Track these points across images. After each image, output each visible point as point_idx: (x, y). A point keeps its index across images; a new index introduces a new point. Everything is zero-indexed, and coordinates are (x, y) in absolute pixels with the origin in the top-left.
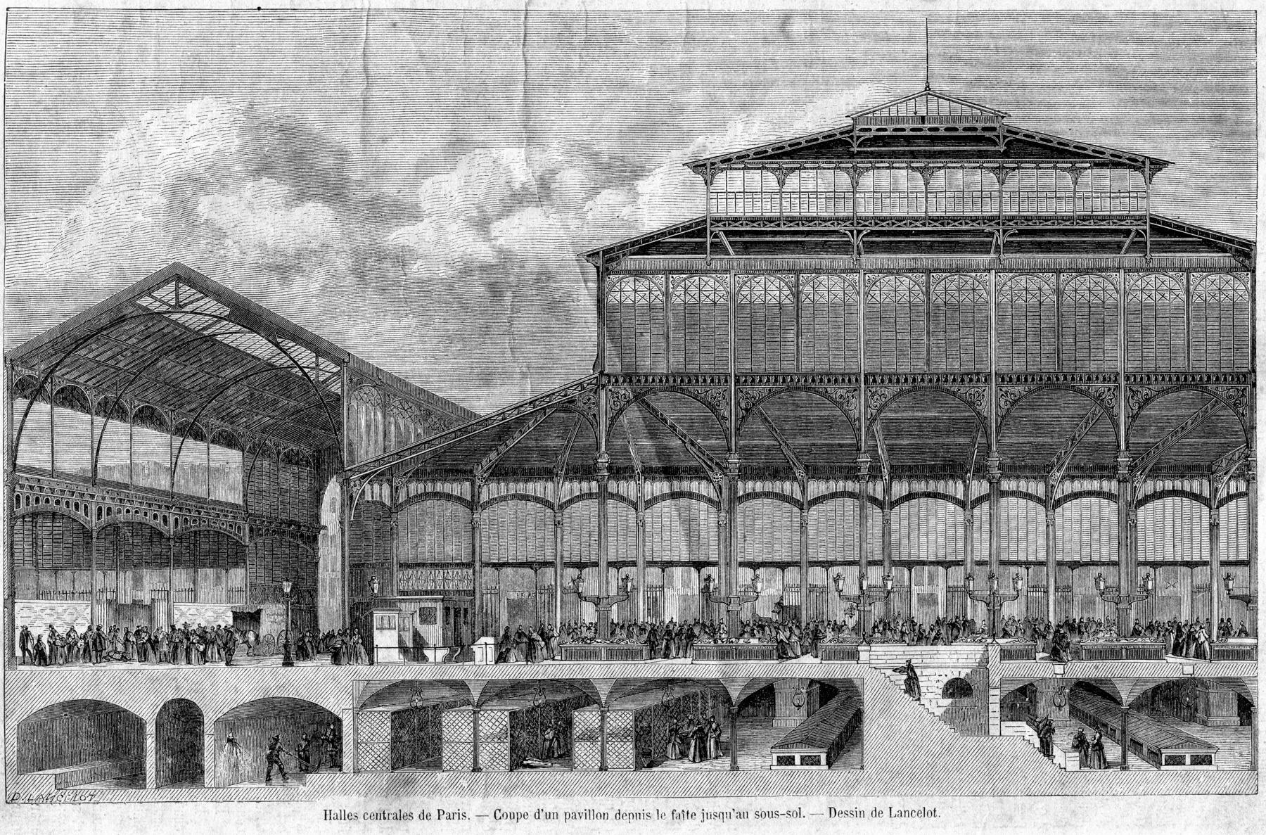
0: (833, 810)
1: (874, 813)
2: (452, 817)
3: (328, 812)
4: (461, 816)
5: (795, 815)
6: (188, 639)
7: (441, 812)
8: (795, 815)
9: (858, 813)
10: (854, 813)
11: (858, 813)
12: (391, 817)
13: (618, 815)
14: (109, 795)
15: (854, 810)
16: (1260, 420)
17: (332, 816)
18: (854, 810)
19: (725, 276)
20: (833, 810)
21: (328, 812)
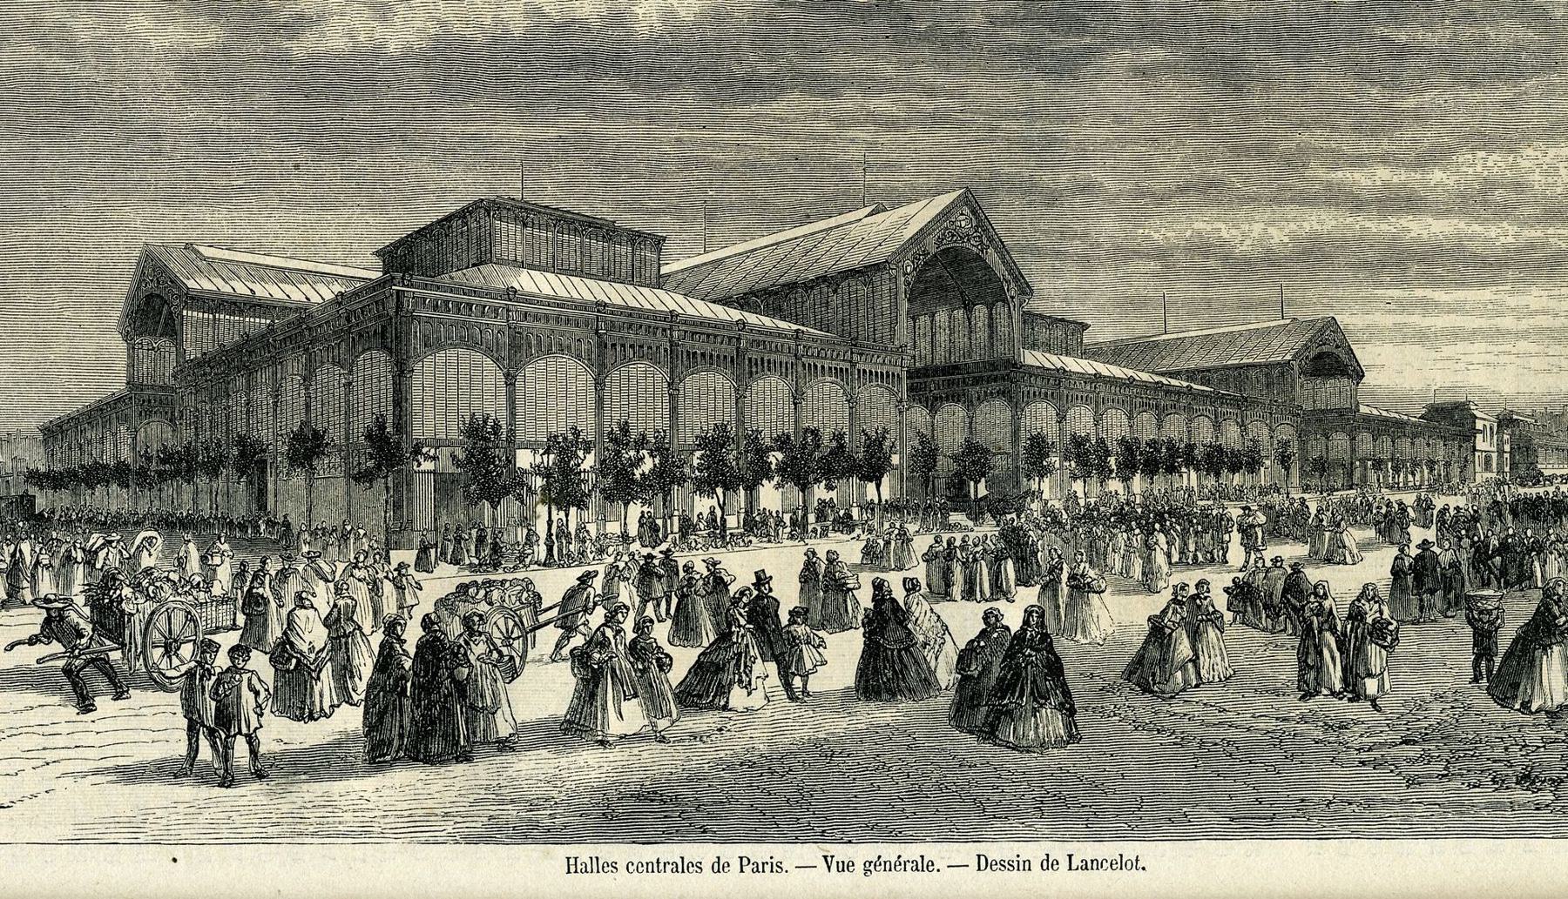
0: (983, 859)
1: (1045, 863)
2: (760, 869)
3: (572, 861)
4: (775, 868)
5: (1129, 866)
6: (203, 667)
7: (745, 861)
8: (1129, 866)
9: (1021, 863)
10: (1015, 864)
11: (1021, 863)
12: (909, 866)
13: (1045, 863)
14: (348, 819)
15: (1015, 859)
16: (1334, 570)
17: (579, 867)
18: (1015, 859)
19: (1009, 517)
20: (983, 859)
21: (572, 861)
